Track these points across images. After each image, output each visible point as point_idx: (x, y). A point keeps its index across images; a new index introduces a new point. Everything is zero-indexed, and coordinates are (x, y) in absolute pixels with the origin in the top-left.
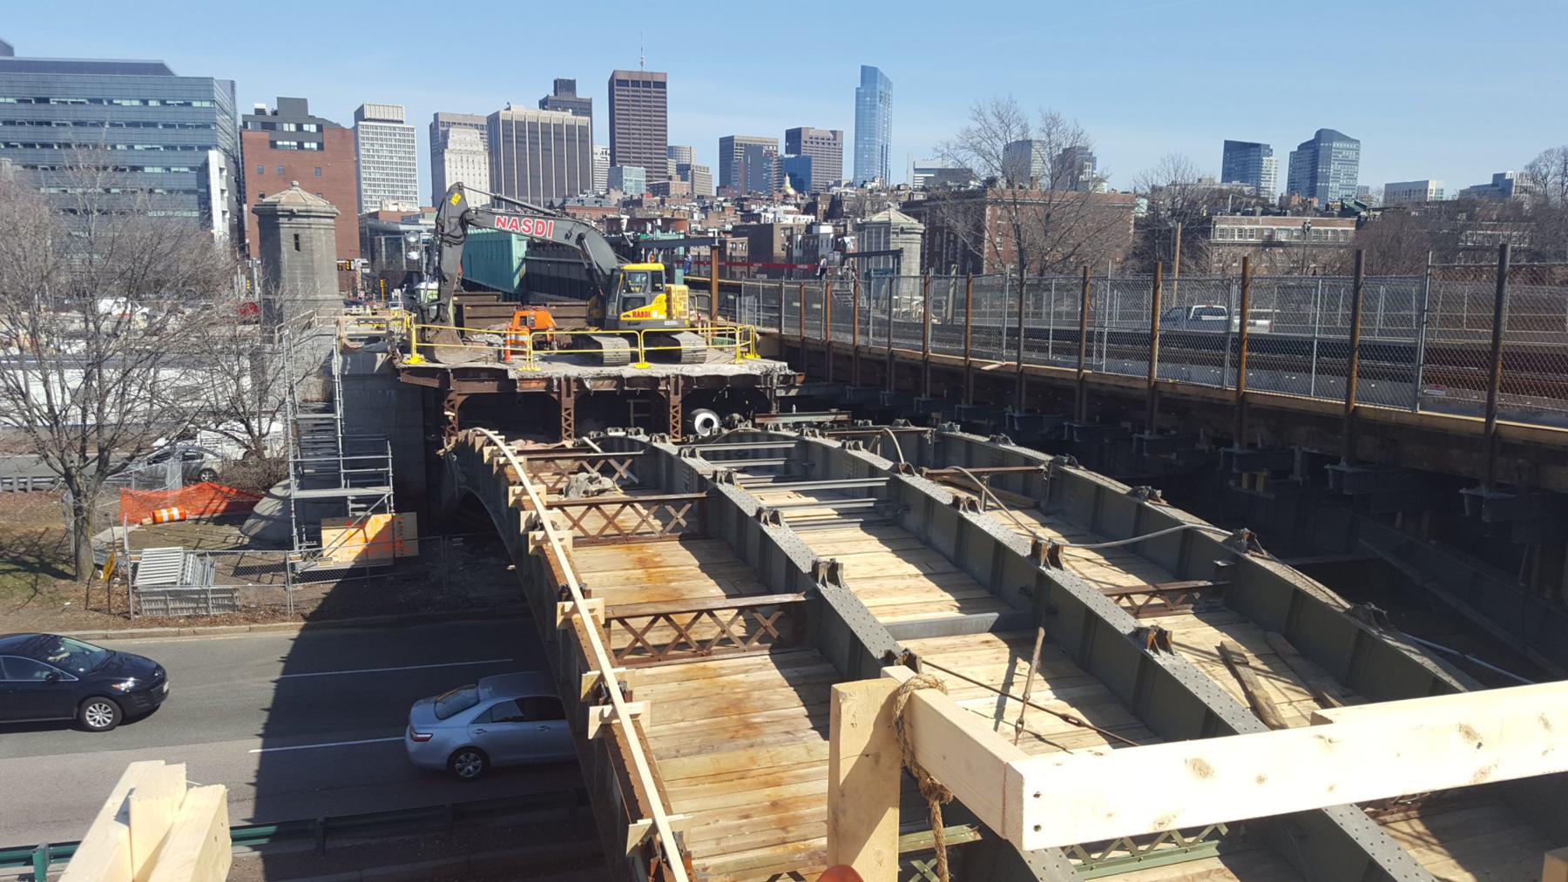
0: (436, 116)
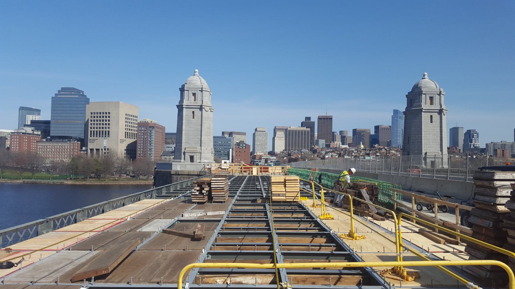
0: (275, 127)
